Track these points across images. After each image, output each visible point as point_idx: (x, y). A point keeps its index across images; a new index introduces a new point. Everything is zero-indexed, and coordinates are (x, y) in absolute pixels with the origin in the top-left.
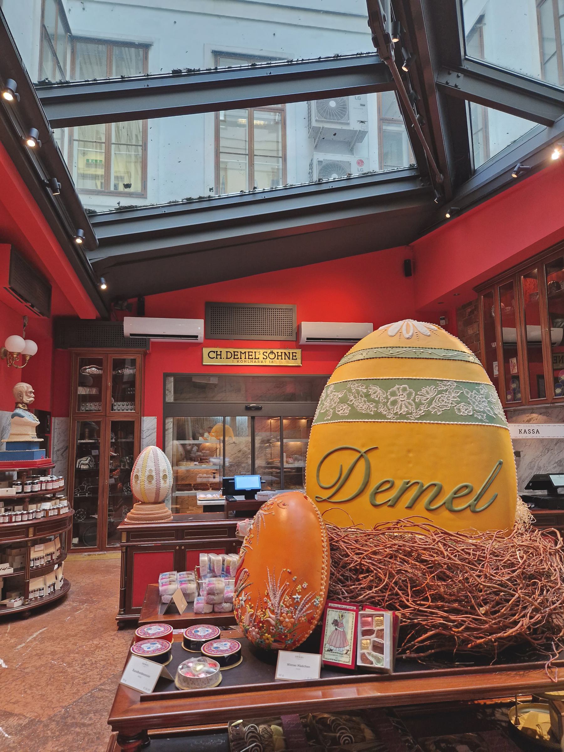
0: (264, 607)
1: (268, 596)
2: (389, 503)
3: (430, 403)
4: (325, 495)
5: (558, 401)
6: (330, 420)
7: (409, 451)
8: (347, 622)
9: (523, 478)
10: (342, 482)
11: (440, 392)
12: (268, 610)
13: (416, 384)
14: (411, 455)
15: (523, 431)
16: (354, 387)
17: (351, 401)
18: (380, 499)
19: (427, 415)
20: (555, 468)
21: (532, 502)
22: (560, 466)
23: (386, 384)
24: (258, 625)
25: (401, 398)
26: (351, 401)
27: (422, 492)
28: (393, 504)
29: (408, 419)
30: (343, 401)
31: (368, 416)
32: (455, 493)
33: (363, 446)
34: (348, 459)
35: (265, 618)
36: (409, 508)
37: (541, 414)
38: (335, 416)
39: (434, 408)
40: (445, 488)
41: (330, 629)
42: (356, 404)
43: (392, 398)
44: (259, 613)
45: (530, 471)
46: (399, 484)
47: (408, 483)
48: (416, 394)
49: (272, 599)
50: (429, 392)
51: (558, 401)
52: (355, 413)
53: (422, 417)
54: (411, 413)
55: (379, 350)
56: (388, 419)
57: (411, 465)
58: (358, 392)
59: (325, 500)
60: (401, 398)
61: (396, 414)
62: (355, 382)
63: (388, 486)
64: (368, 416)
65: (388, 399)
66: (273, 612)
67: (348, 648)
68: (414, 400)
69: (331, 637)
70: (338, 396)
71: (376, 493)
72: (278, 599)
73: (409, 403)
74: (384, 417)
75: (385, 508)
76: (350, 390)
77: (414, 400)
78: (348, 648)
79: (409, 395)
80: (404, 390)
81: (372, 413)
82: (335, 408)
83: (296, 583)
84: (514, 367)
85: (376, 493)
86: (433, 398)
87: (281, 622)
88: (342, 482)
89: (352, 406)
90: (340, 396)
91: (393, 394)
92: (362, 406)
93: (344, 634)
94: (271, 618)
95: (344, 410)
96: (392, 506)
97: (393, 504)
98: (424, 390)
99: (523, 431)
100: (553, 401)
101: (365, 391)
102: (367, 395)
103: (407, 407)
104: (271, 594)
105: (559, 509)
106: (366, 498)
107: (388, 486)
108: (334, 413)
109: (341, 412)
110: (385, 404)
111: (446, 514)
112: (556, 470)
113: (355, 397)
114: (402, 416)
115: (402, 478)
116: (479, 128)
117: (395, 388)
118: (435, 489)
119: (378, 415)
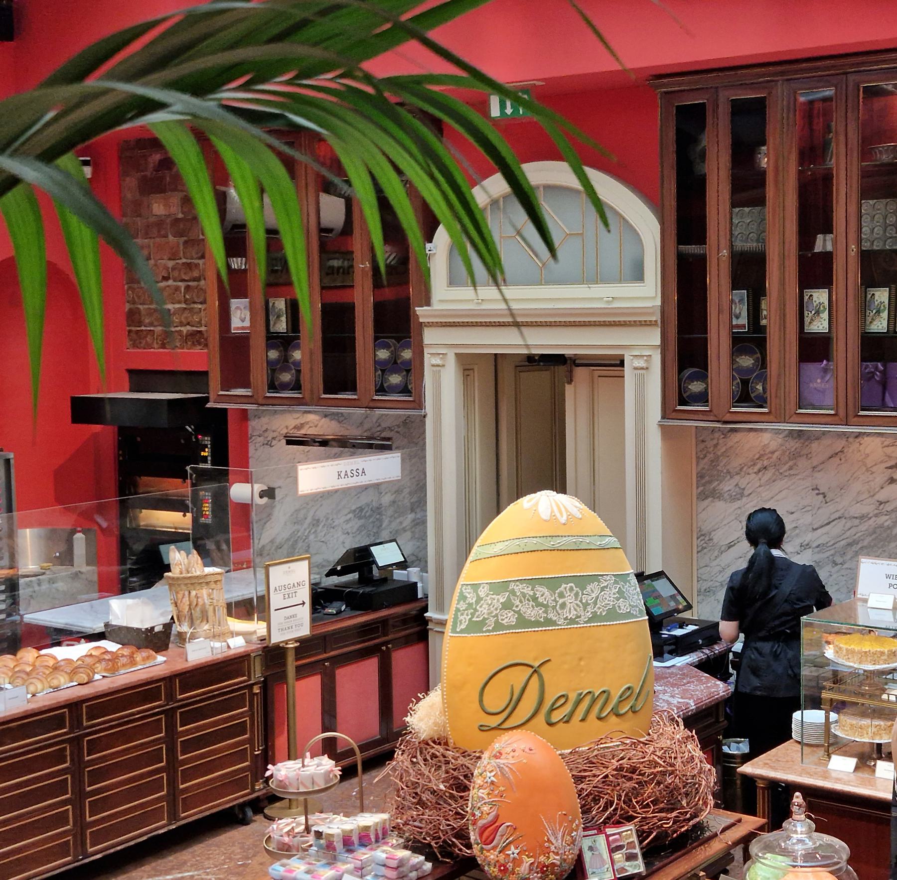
0: (546, 852)
1: (549, 841)
2: (565, 719)
3: (595, 603)
4: (494, 721)
5: (379, 405)
6: (492, 631)
7: (581, 659)
8: (600, 844)
9: (278, 541)
10: (514, 704)
11: (602, 589)
12: (551, 854)
13: (582, 581)
14: (582, 663)
15: (343, 475)
16: (519, 588)
17: (517, 606)
18: (556, 716)
19: (595, 617)
20: (348, 521)
21: (341, 600)
22: (360, 518)
23: (552, 583)
24: (542, 869)
25: (569, 599)
26: (517, 606)
27: (594, 701)
28: (567, 720)
29: (578, 623)
30: (507, 606)
31: (537, 624)
32: (621, 697)
33: (535, 659)
34: (519, 676)
35: (550, 861)
36: (583, 720)
37: (326, 416)
38: (498, 626)
39: (599, 608)
40: (612, 693)
41: (587, 856)
42: (523, 610)
43: (561, 601)
44: (542, 859)
45: (296, 527)
46: (573, 697)
47: (581, 694)
48: (583, 594)
49: (554, 842)
50: (593, 589)
51: (379, 405)
52: (523, 622)
53: (590, 620)
54: (580, 617)
55: (538, 540)
56: (559, 625)
57: (583, 675)
58: (524, 595)
59: (493, 729)
60: (569, 599)
61: (566, 619)
62: (518, 583)
63: (562, 701)
64: (537, 624)
65: (556, 602)
66: (557, 854)
67: (607, 866)
68: (581, 601)
69: (590, 862)
70: (498, 600)
71: (552, 709)
72: (560, 841)
73: (577, 605)
74: (554, 623)
75: (561, 724)
76: (513, 592)
77: (581, 601)
78: (607, 866)
79: (576, 595)
80: (571, 589)
81: (542, 620)
82: (496, 616)
83: (572, 821)
84: (279, 317)
85: (552, 709)
86: (597, 597)
87: (565, 860)
88: (514, 704)
89: (518, 612)
90: (502, 600)
91: (561, 595)
92: (531, 612)
93: (600, 855)
94: (554, 859)
95: (509, 618)
96: (567, 722)
97: (567, 720)
98: (588, 588)
99: (343, 475)
100: (371, 405)
101: (531, 593)
102: (535, 599)
103: (576, 610)
104: (552, 839)
105: (388, 607)
106: (541, 718)
107: (562, 701)
108: (497, 622)
109: (506, 620)
110: (554, 607)
111: (613, 719)
112: (350, 525)
113: (521, 602)
114: (572, 621)
115: (575, 690)
116: (574, 182)
117: (562, 589)
118: (605, 695)
119: (549, 622)
